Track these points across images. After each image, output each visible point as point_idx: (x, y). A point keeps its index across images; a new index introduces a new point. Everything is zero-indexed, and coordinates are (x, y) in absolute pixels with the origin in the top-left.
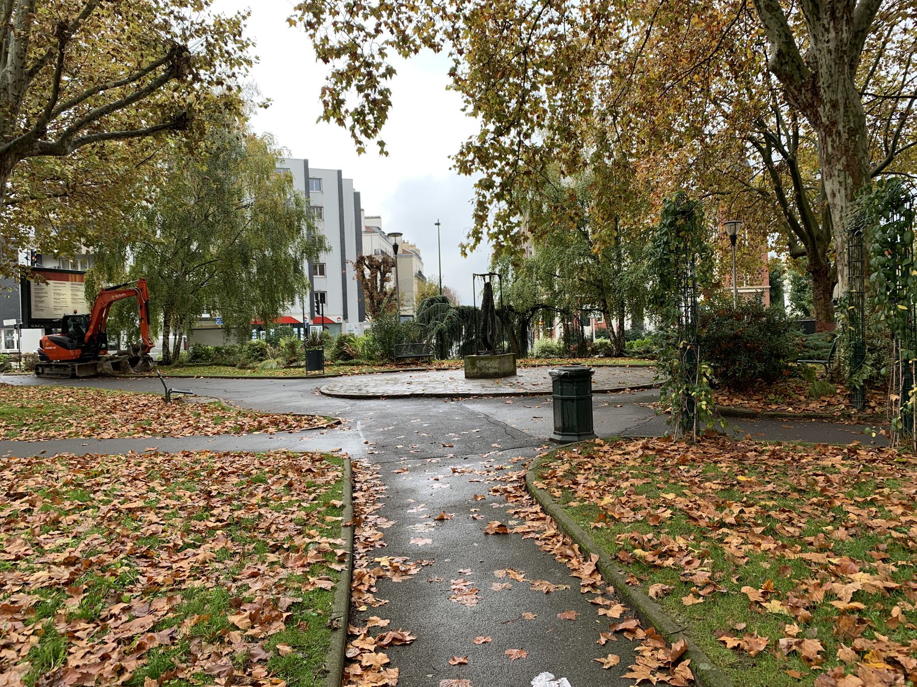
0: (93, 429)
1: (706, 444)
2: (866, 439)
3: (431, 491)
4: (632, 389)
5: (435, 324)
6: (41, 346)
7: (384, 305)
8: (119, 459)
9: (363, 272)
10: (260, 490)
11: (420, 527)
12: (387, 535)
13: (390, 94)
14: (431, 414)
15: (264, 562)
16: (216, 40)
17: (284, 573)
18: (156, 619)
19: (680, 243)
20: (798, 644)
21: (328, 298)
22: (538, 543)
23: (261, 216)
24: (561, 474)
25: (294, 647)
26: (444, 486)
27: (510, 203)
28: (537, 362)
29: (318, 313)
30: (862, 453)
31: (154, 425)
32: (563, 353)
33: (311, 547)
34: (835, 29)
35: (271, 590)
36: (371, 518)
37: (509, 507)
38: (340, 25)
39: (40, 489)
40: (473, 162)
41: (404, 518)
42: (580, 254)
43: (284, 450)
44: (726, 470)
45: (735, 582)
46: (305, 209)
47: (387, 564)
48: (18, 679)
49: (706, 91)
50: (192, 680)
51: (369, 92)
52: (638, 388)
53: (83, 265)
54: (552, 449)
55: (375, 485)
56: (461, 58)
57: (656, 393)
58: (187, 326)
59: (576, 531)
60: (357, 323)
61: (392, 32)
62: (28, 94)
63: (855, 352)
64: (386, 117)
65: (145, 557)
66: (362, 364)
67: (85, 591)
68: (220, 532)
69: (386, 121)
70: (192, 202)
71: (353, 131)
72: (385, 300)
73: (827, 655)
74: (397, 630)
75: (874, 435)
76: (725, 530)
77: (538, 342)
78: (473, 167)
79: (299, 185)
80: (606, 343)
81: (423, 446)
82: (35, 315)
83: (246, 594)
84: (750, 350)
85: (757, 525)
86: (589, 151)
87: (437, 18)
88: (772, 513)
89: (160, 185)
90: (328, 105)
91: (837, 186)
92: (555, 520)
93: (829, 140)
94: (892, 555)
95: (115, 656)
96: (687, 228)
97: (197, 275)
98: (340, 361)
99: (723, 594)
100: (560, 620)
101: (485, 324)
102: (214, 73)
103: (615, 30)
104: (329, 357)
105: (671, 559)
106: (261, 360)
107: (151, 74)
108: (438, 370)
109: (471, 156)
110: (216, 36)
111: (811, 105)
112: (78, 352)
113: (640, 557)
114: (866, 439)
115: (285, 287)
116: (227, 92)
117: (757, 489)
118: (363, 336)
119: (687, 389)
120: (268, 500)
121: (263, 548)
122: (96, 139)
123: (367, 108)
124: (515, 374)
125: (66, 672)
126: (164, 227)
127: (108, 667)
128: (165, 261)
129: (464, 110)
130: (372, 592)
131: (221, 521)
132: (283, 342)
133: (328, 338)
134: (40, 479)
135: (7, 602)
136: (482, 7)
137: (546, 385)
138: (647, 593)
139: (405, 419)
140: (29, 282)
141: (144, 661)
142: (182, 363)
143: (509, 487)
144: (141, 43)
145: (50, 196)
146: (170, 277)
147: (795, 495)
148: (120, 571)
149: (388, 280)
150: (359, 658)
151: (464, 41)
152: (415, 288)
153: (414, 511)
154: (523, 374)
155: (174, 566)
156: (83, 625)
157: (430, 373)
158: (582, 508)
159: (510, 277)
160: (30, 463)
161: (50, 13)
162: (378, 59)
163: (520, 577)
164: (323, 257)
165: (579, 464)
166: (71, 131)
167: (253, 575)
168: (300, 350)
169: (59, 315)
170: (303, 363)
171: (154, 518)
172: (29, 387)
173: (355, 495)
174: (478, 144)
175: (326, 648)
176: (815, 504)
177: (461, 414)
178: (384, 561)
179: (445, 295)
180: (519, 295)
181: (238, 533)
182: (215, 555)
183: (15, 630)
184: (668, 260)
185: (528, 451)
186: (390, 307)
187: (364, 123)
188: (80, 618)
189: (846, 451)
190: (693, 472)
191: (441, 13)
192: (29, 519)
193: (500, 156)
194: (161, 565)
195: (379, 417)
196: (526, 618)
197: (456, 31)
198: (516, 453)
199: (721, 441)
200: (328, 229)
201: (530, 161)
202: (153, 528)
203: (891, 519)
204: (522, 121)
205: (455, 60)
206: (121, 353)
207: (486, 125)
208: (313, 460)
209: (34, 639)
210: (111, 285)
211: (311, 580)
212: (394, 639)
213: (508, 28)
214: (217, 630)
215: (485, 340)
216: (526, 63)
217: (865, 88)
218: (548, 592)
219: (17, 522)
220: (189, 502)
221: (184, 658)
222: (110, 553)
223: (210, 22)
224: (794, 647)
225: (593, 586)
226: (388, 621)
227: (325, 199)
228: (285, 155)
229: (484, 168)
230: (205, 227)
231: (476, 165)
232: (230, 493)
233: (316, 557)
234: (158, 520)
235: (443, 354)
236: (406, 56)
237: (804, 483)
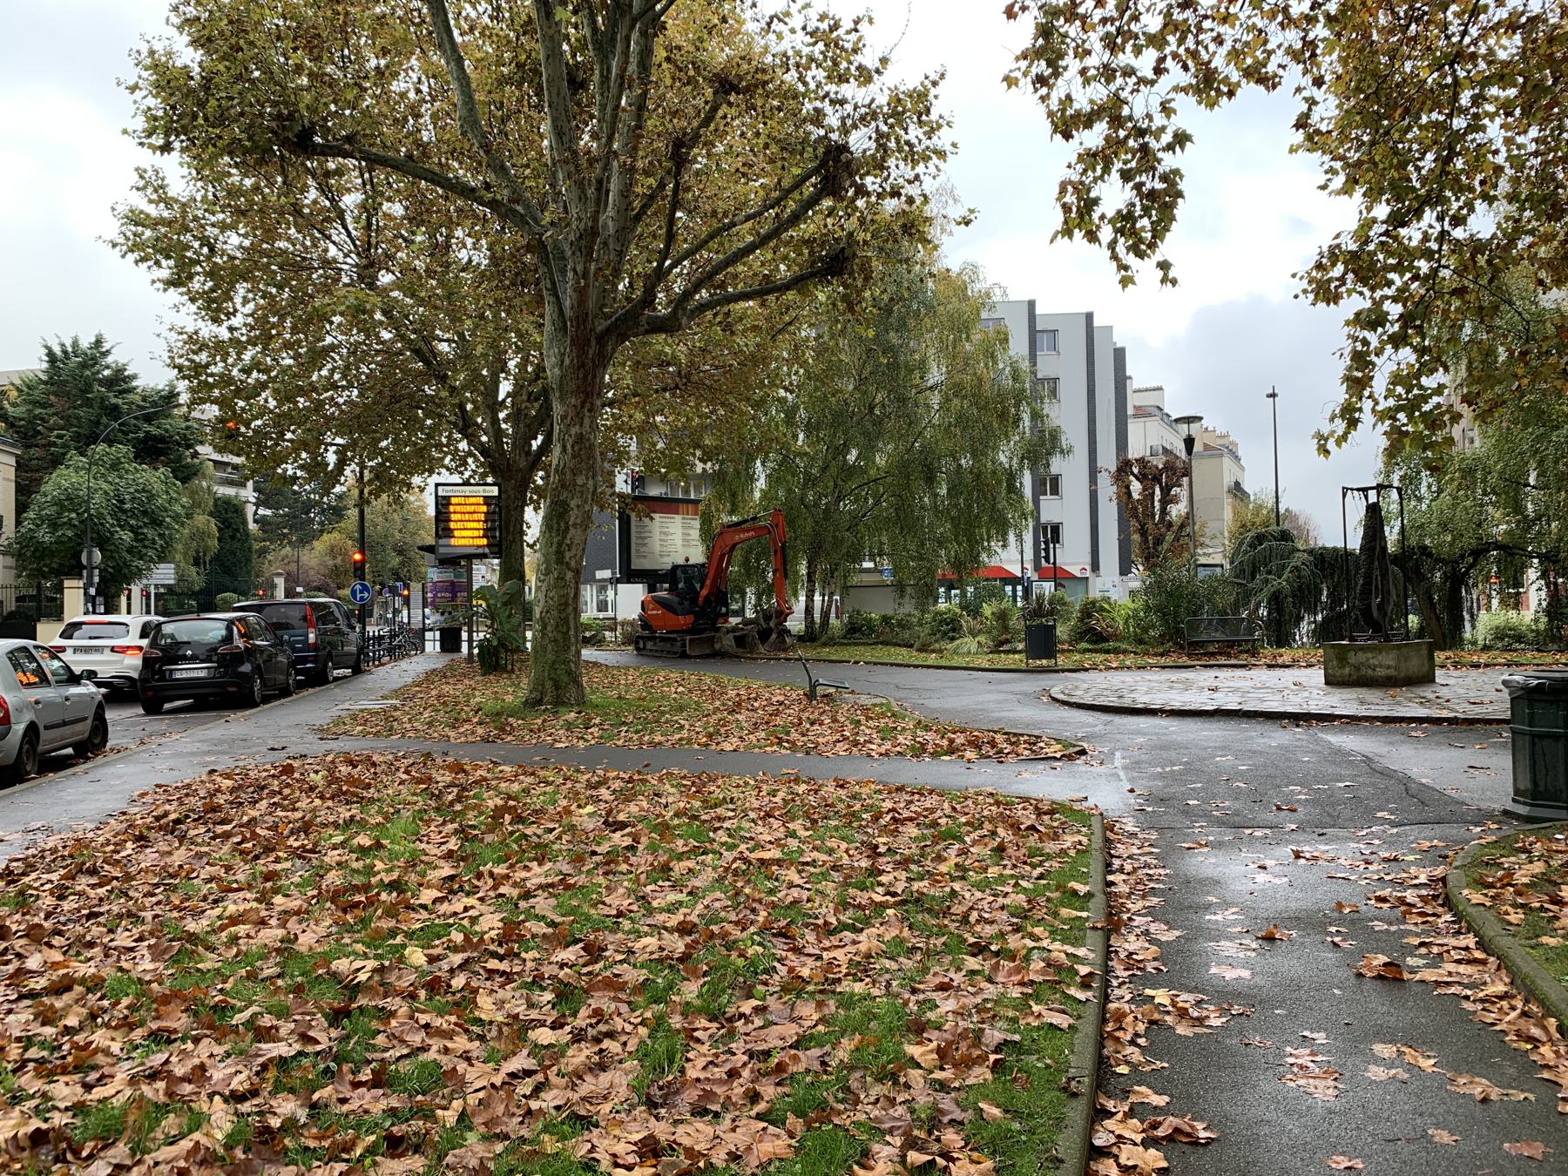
0: (710, 736)
3: (1251, 886)
5: (1267, 581)
6: (643, 608)
7: (1165, 546)
8: (747, 784)
9: (1128, 487)
10: (953, 851)
11: (1228, 948)
12: (1167, 952)
15: (959, 969)
16: (892, 127)
17: (991, 991)
18: (800, 1031)
21: (1065, 534)
23: (956, 401)
24: (1526, 880)
25: (1006, 1111)
26: (1277, 881)
27: (1421, 351)
28: (1484, 659)
29: (1047, 560)
31: (794, 735)
33: (1035, 955)
35: (970, 1015)
36: (1138, 920)
39: (645, 818)
40: (1342, 280)
41: (1199, 928)
43: (990, 790)
46: (1027, 386)
47: (1167, 1001)
48: (625, 1083)
50: (853, 1131)
51: (1144, 178)
53: (697, 490)
55: (1147, 866)
56: (1318, 94)
58: (840, 583)
60: (1116, 577)
61: (1185, 68)
62: (633, 246)
64: (1173, 219)
65: (785, 936)
66: (1125, 652)
67: (705, 974)
68: (890, 912)
69: (1174, 225)
70: (851, 387)
72: (1169, 537)
74: (1183, 1117)
78: (1343, 289)
79: (1018, 346)
81: (1238, 805)
82: (637, 564)
83: (931, 1015)
89: (804, 364)
90: (1070, 210)
95: (746, 1073)
97: (856, 501)
98: (1084, 645)
101: (1368, 583)
102: (886, 180)
104: (1065, 637)
106: (953, 639)
107: (796, 195)
108: (1270, 666)
109: (1338, 270)
110: (891, 121)
112: (690, 619)
115: (991, 517)
116: (906, 207)
118: (1125, 601)
120: (966, 870)
121: (956, 946)
122: (719, 303)
123: (1138, 208)
124: (1433, 681)
125: (684, 1084)
126: (809, 428)
127: (738, 1090)
128: (810, 481)
129: (1323, 187)
130: (1138, 1046)
131: (894, 894)
132: (987, 610)
134: (645, 804)
135: (608, 973)
137: (1500, 706)
139: (1204, 754)
140: (629, 517)
141: (786, 1090)
142: (832, 639)
143: (1410, 895)
144: (783, 149)
145: (657, 391)
146: (816, 505)
148: (750, 952)
149: (1175, 500)
150: (1115, 1150)
151: (1328, 59)
152: (1228, 514)
153: (1219, 917)
154: (1451, 681)
155: (825, 954)
156: (704, 1023)
157: (1254, 673)
159: (1424, 489)
160: (631, 780)
161: (663, 124)
162: (1159, 120)
163: (1426, 1064)
164: (1057, 465)
166: (687, 294)
167: (943, 987)
168: (1015, 622)
169: (666, 563)
170: (1021, 646)
171: (797, 879)
172: (627, 668)
173: (1110, 878)
174: (1353, 247)
175: (1059, 1123)
177: (1313, 752)
178: (1162, 996)
179: (1286, 526)
181: (920, 917)
182: (884, 947)
183: (619, 1014)
185: (1455, 831)
186: (1178, 549)
187: (1134, 233)
188: (700, 1011)
191: (1280, 18)
192: (633, 860)
194: (806, 951)
195: (1154, 747)
196: (1437, 1139)
197: (1310, 45)
200: (1066, 416)
201: (1466, 269)
202: (795, 893)
204: (1448, 194)
206: (747, 622)
207: (1369, 209)
208: (1039, 813)
209: (643, 1031)
210: (735, 519)
211: (1036, 1008)
212: (1177, 1130)
213: (1418, 20)
214: (889, 1062)
215: (1367, 612)
216: (1456, 82)
218: (1485, 1100)
219: (617, 863)
220: (846, 860)
221: (840, 1095)
222: (737, 923)
223: (882, 100)
226: (1167, 1099)
227: (1064, 365)
228: (997, 296)
229: (1366, 291)
230: (869, 426)
231: (1349, 285)
232: (907, 852)
233: (1043, 972)
234: (801, 882)
235: (1282, 638)
236: (1212, 105)
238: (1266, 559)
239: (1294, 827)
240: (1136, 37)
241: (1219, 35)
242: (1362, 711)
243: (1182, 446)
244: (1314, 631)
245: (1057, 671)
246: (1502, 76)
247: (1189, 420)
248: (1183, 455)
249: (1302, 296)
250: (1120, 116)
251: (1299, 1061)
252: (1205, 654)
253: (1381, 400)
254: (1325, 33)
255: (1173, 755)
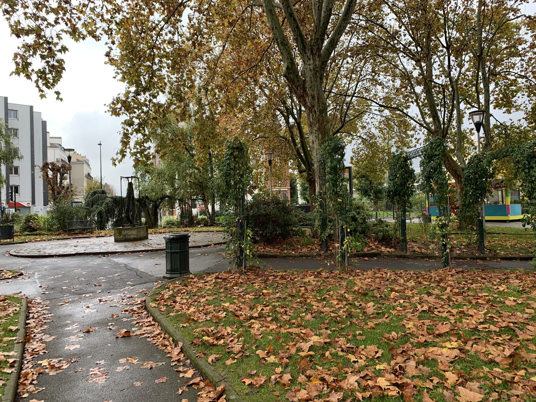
1: (249, 273)
2: (325, 267)
3: (83, 314)
4: (215, 244)
5: (97, 207)
7: (61, 195)
9: (47, 173)
11: (73, 338)
12: (48, 346)
13: (64, 63)
14: (89, 265)
19: (236, 164)
20: (280, 377)
21: (21, 190)
22: (149, 340)
24: (167, 297)
26: (93, 311)
28: (163, 231)
30: (323, 274)
32: (180, 224)
34: (313, 59)
37: (134, 320)
38: (29, 15)
40: (121, 109)
41: (63, 334)
42: (189, 167)
44: (257, 287)
45: (254, 349)
49: (256, 81)
51: (50, 59)
52: (218, 244)
54: (164, 282)
55: (44, 314)
57: (223, 246)
59: (171, 329)
61: (67, 24)
63: (323, 222)
66: (43, 235)
69: (61, 79)
71: (37, 84)
72: (63, 192)
73: (293, 381)
75: (329, 264)
76: (253, 321)
77: (164, 218)
78: (120, 112)
80: (205, 218)
81: (81, 286)
84: (274, 222)
85: (269, 316)
86: (193, 107)
87: (98, 20)
88: (277, 309)
90: (19, 65)
91: (314, 138)
92: (160, 325)
93: (311, 114)
94: (330, 326)
96: (239, 157)
98: (27, 233)
99: (247, 356)
100: (157, 384)
101: (128, 208)
103: (207, 42)
104: (18, 230)
105: (222, 340)
108: (97, 237)
109: (119, 106)
111: (303, 96)
113: (206, 341)
114: (325, 267)
117: (272, 296)
119: (240, 244)
123: (47, 70)
124: (147, 238)
129: (115, 78)
133: (18, 217)
136: (127, 18)
138: (207, 361)
143: (135, 308)
147: (290, 298)
149: (65, 179)
152: (85, 184)
153: (70, 328)
154: (153, 238)
158: (176, 317)
163: (135, 362)
164: (16, 162)
165: (178, 290)
173: (28, 322)
174: (124, 99)
176: (298, 302)
177: (109, 265)
178: (45, 363)
180: (152, 190)
184: (230, 173)
185: (149, 285)
187: (45, 79)
189: (316, 273)
190: (241, 290)
193: (138, 107)
195: (52, 269)
197: (111, 30)
198: (142, 287)
199: (257, 272)
201: (157, 112)
203: (332, 307)
205: (109, 47)
207: (129, 88)
213: (144, 32)
217: (332, 89)
218: (151, 368)
224: (278, 379)
225: (178, 361)
229: (128, 113)
235: (102, 226)
237: (294, 292)
238: (98, 199)
239: (100, 291)
240: (47, 7)
241: (79, 17)
242: (125, 250)
243: (67, 158)
244: (113, 224)
245: (14, 244)
246: (167, 56)
247: (69, 150)
248: (67, 162)
249: (107, 112)
250: (40, 35)
251: (94, 373)
252: (74, 234)
253: (132, 149)
254: (115, 27)
255: (58, 271)
